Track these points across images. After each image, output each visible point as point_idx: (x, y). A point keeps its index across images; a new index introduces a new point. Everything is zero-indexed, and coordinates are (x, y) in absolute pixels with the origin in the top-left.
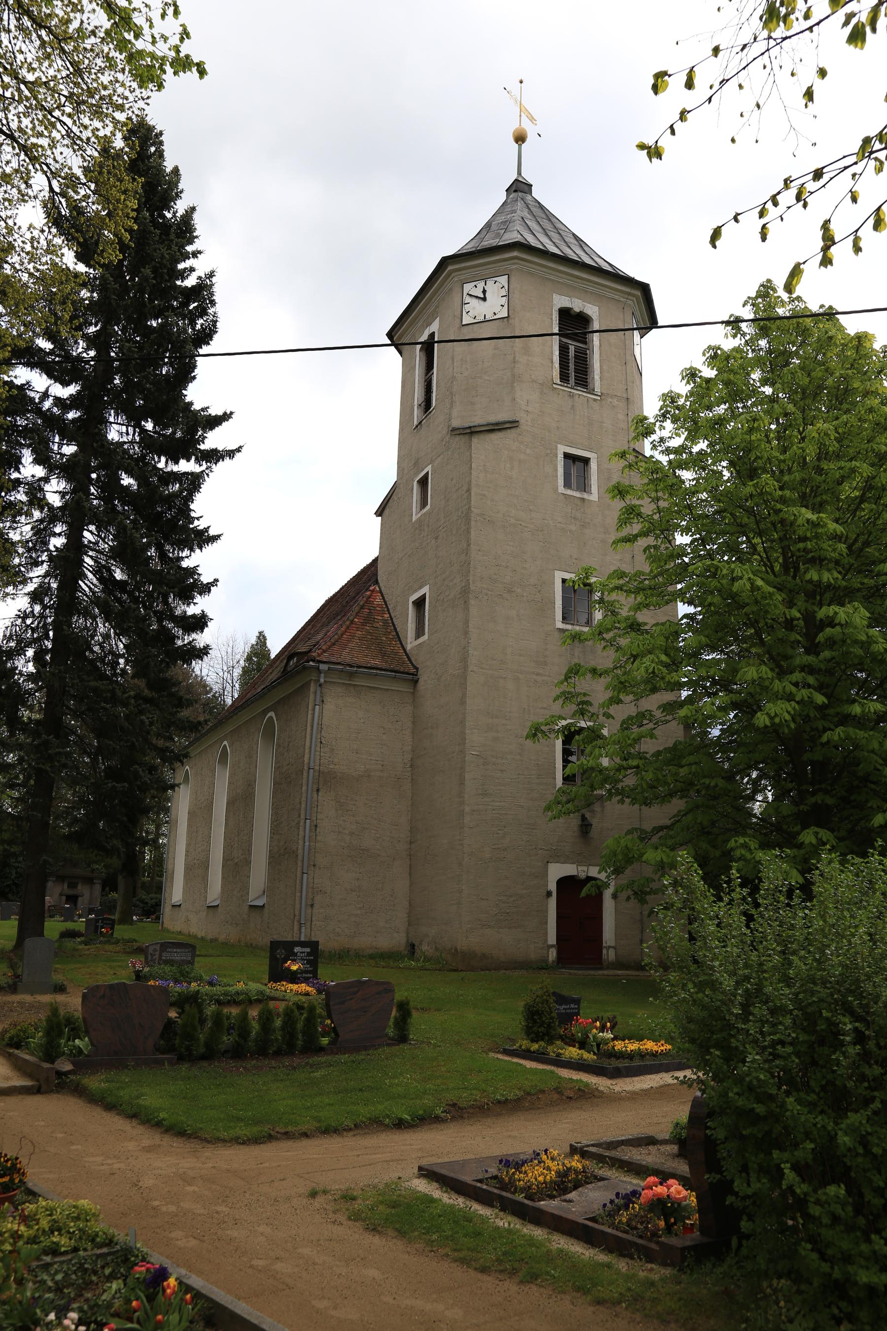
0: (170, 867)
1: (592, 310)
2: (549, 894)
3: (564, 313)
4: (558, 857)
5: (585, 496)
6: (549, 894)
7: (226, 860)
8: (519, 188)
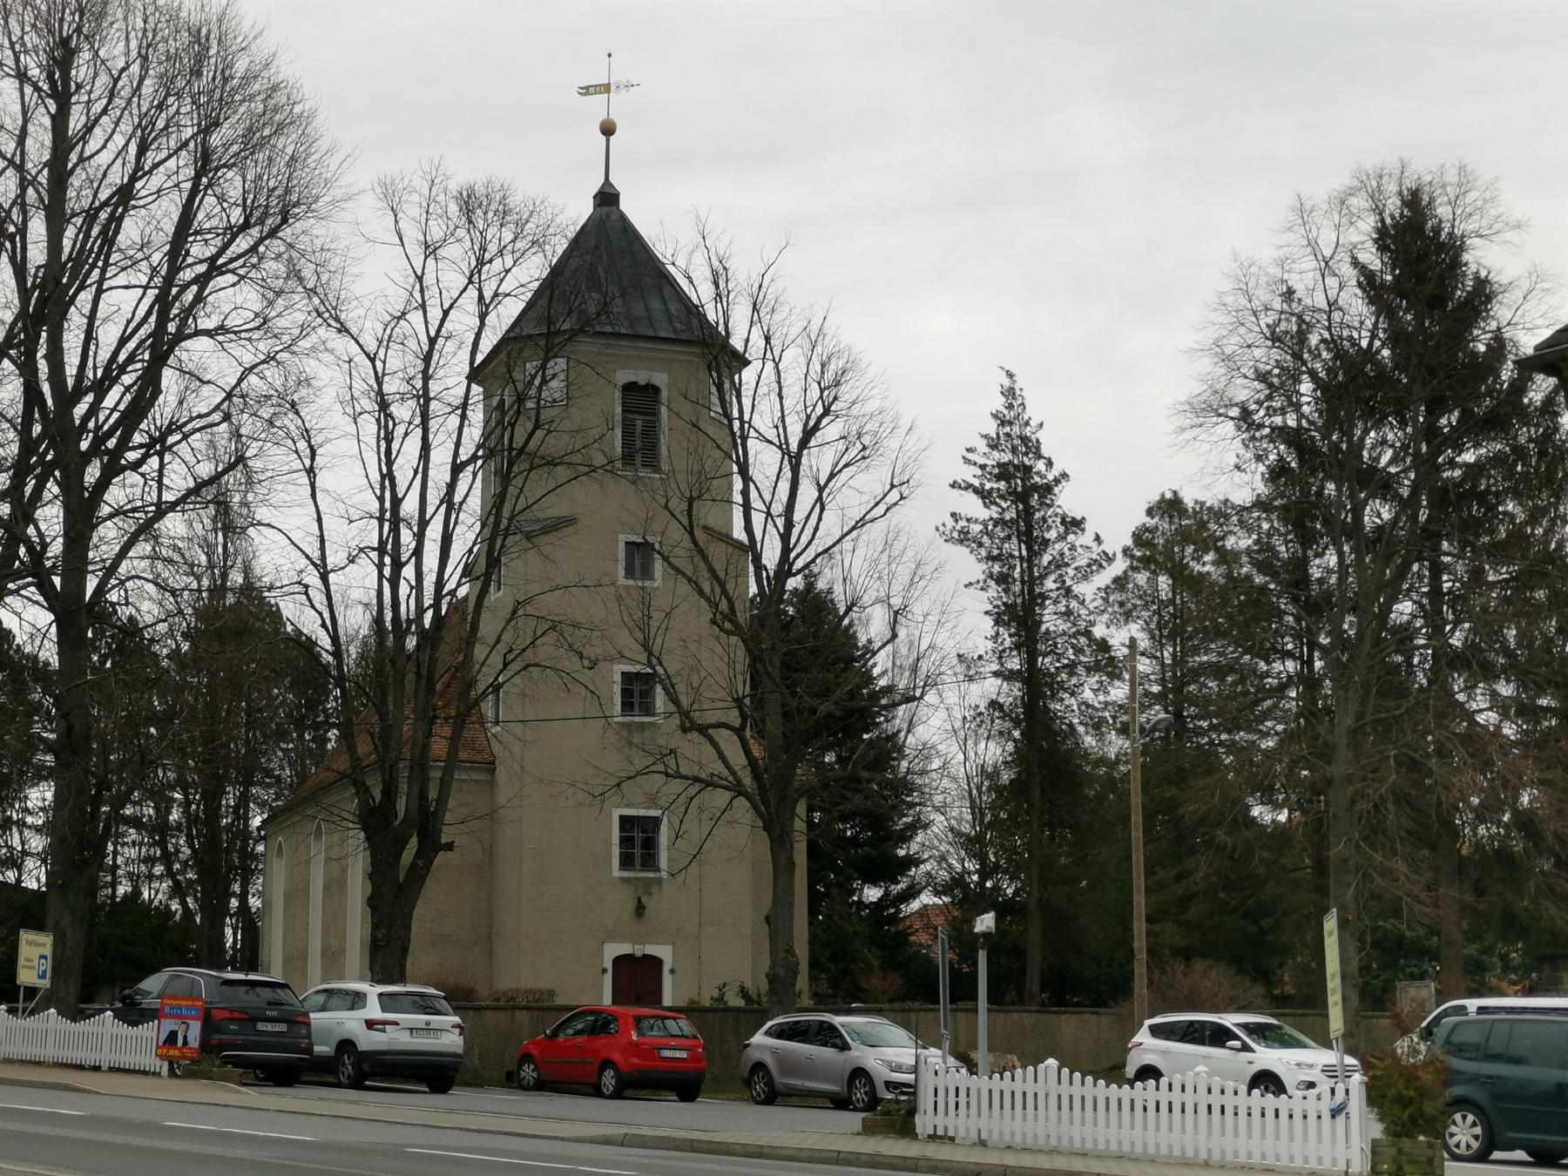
0: (265, 958)
1: (660, 379)
2: (604, 971)
3: (629, 388)
4: (613, 937)
5: (648, 583)
6: (604, 971)
7: (324, 949)
8: (607, 198)
